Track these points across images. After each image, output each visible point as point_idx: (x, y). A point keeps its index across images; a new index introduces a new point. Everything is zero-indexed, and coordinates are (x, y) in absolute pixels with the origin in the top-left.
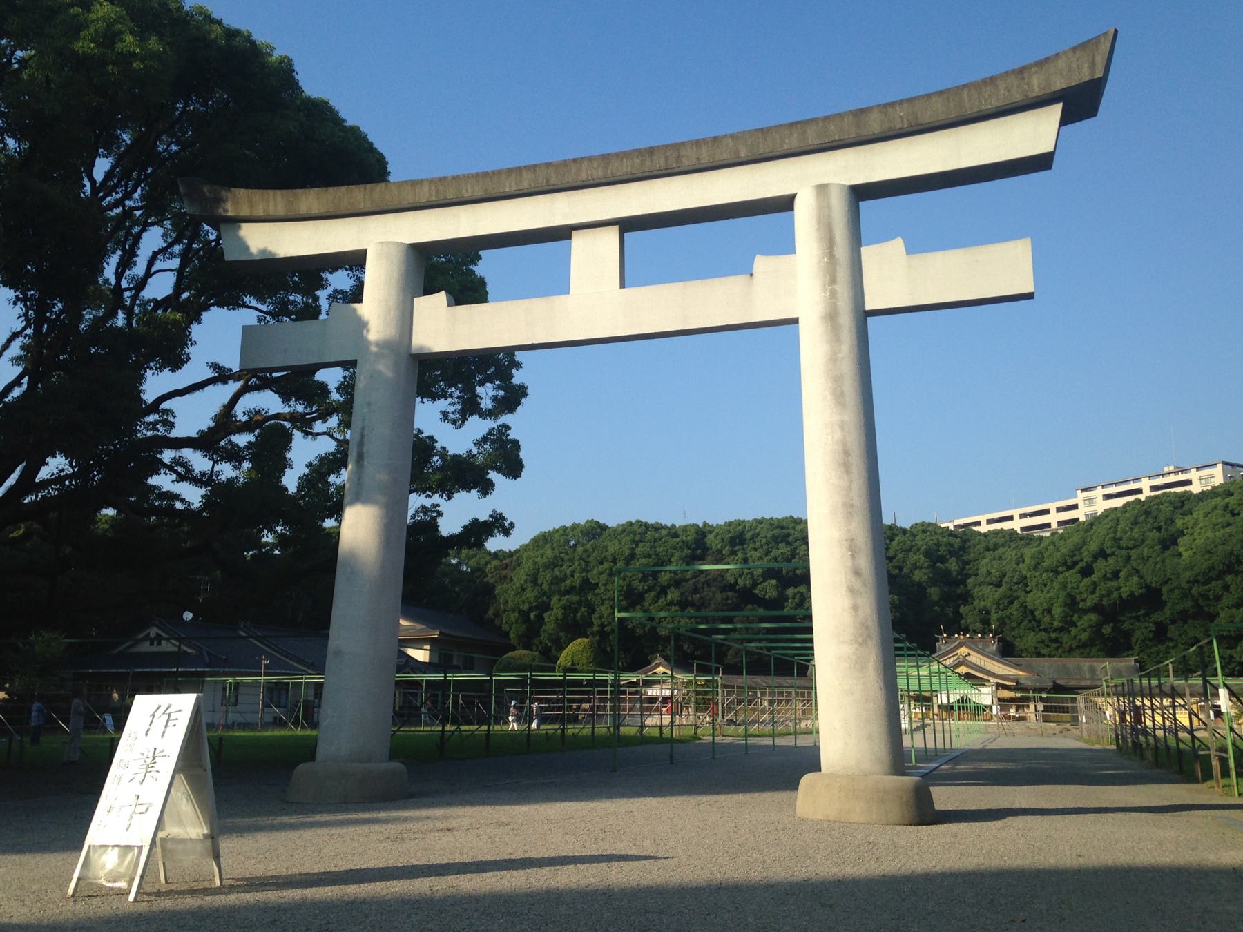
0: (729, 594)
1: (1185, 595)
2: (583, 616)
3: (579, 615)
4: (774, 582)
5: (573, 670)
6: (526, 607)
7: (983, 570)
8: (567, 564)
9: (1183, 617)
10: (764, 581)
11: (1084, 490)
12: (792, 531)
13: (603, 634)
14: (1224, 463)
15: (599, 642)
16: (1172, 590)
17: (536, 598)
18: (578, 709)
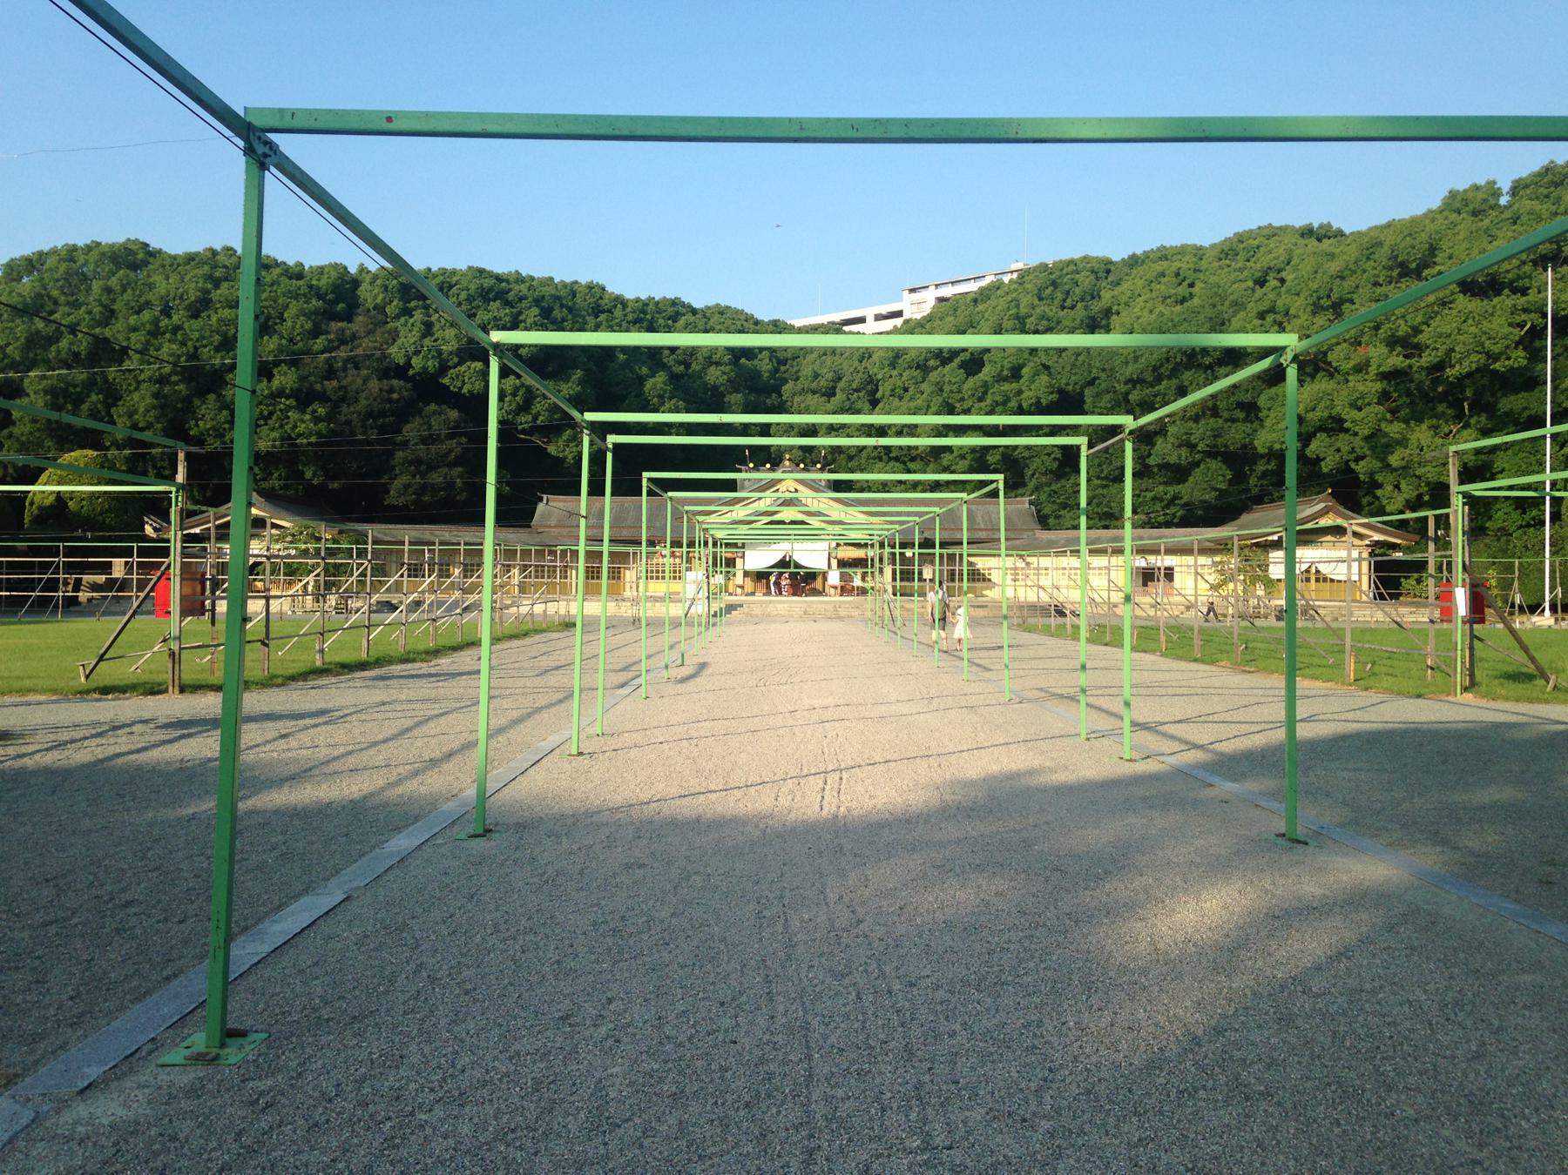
0: (395, 382)
10: (460, 364)
11: (913, 291)
18: (78, 583)
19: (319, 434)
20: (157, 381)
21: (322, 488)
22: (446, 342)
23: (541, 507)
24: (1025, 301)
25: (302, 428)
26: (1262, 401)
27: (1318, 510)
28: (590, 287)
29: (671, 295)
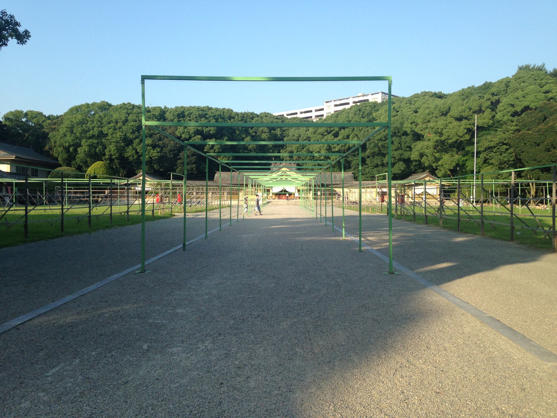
1: (376, 145)
2: (100, 150)
3: (97, 149)
4: (199, 136)
5: (95, 177)
6: (67, 145)
7: (291, 134)
8: (90, 123)
9: (374, 155)
11: (326, 102)
12: (208, 113)
13: (111, 160)
14: (383, 93)
15: (109, 164)
16: (370, 144)
17: (73, 140)
19: (158, 156)
20: (116, 142)
21: (159, 170)
22: (191, 130)
23: (216, 175)
24: (350, 116)
25: (154, 155)
26: (412, 146)
27: (425, 176)
28: (229, 110)
29: (251, 111)
